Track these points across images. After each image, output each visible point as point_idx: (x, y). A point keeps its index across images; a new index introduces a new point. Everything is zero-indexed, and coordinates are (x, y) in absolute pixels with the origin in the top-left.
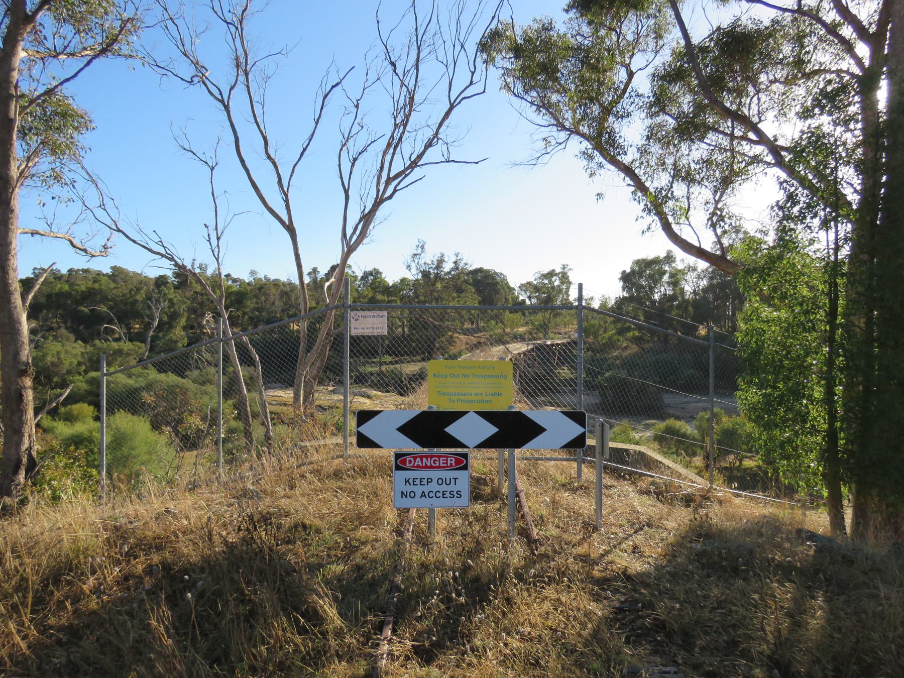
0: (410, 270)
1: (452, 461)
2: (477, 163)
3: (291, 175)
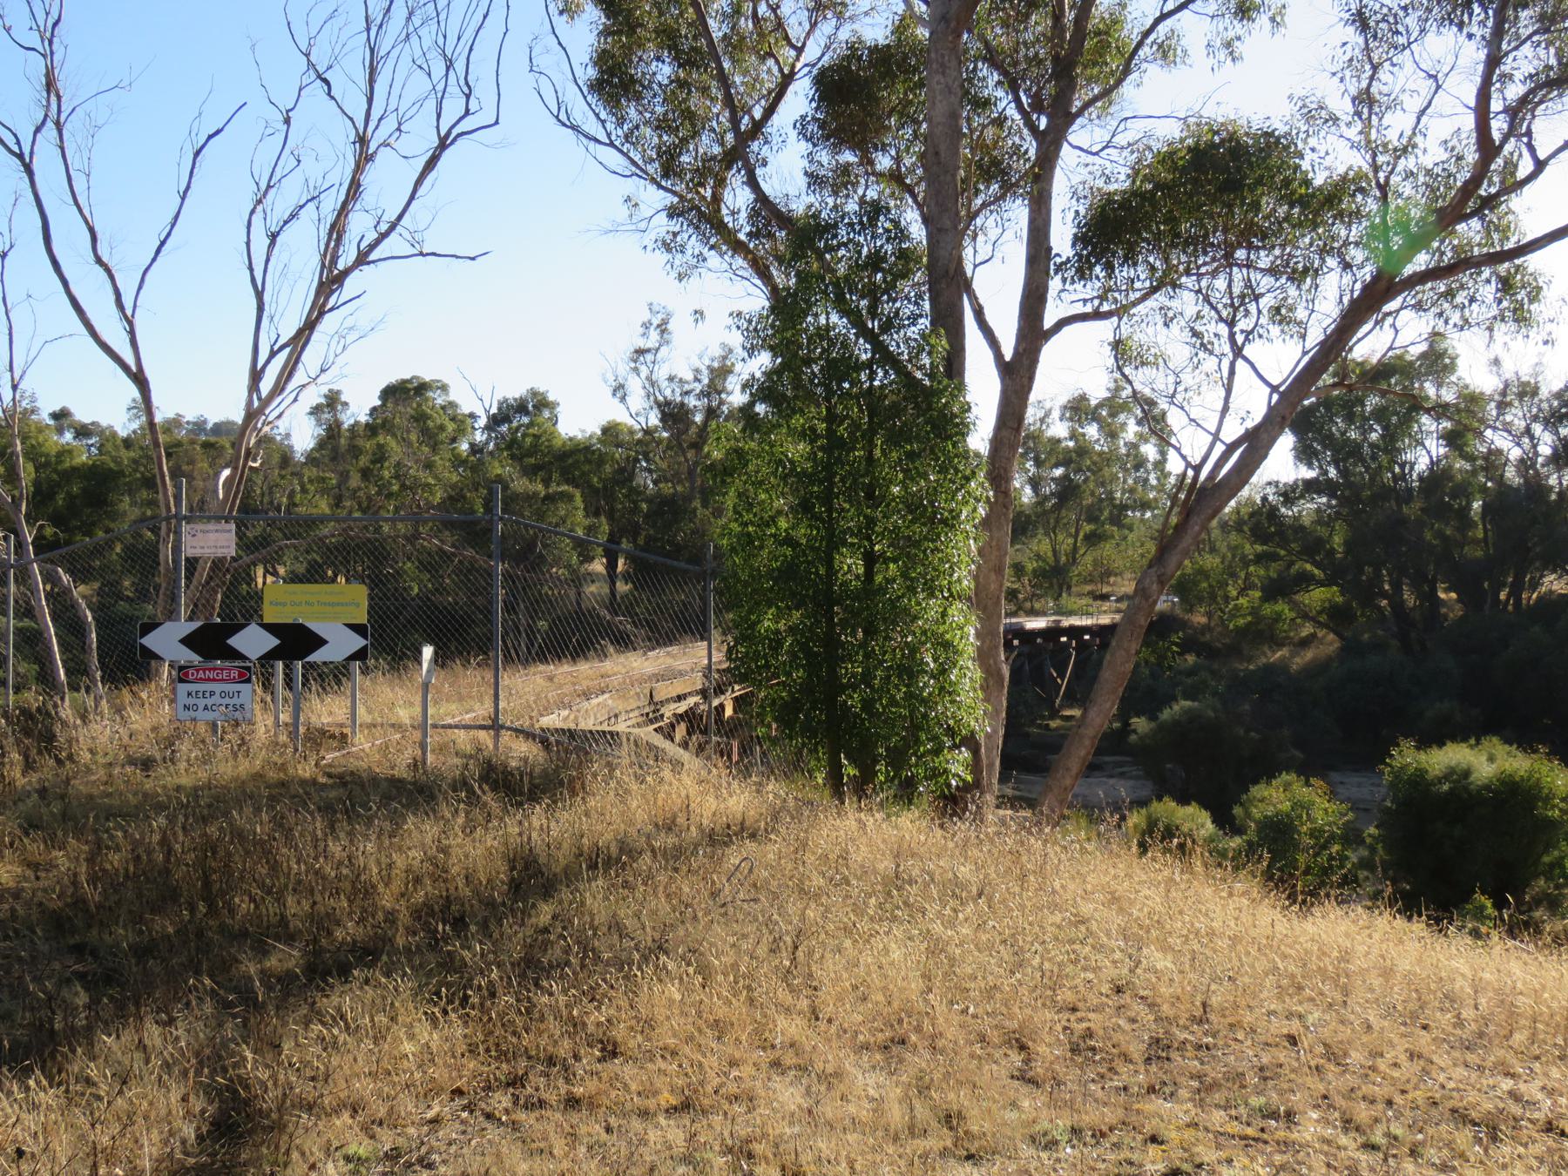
0: (623, 399)
1: (234, 674)
2: (473, 259)
3: (140, 288)
